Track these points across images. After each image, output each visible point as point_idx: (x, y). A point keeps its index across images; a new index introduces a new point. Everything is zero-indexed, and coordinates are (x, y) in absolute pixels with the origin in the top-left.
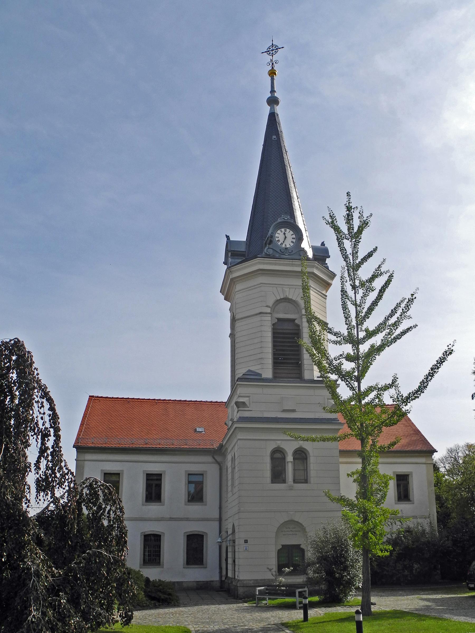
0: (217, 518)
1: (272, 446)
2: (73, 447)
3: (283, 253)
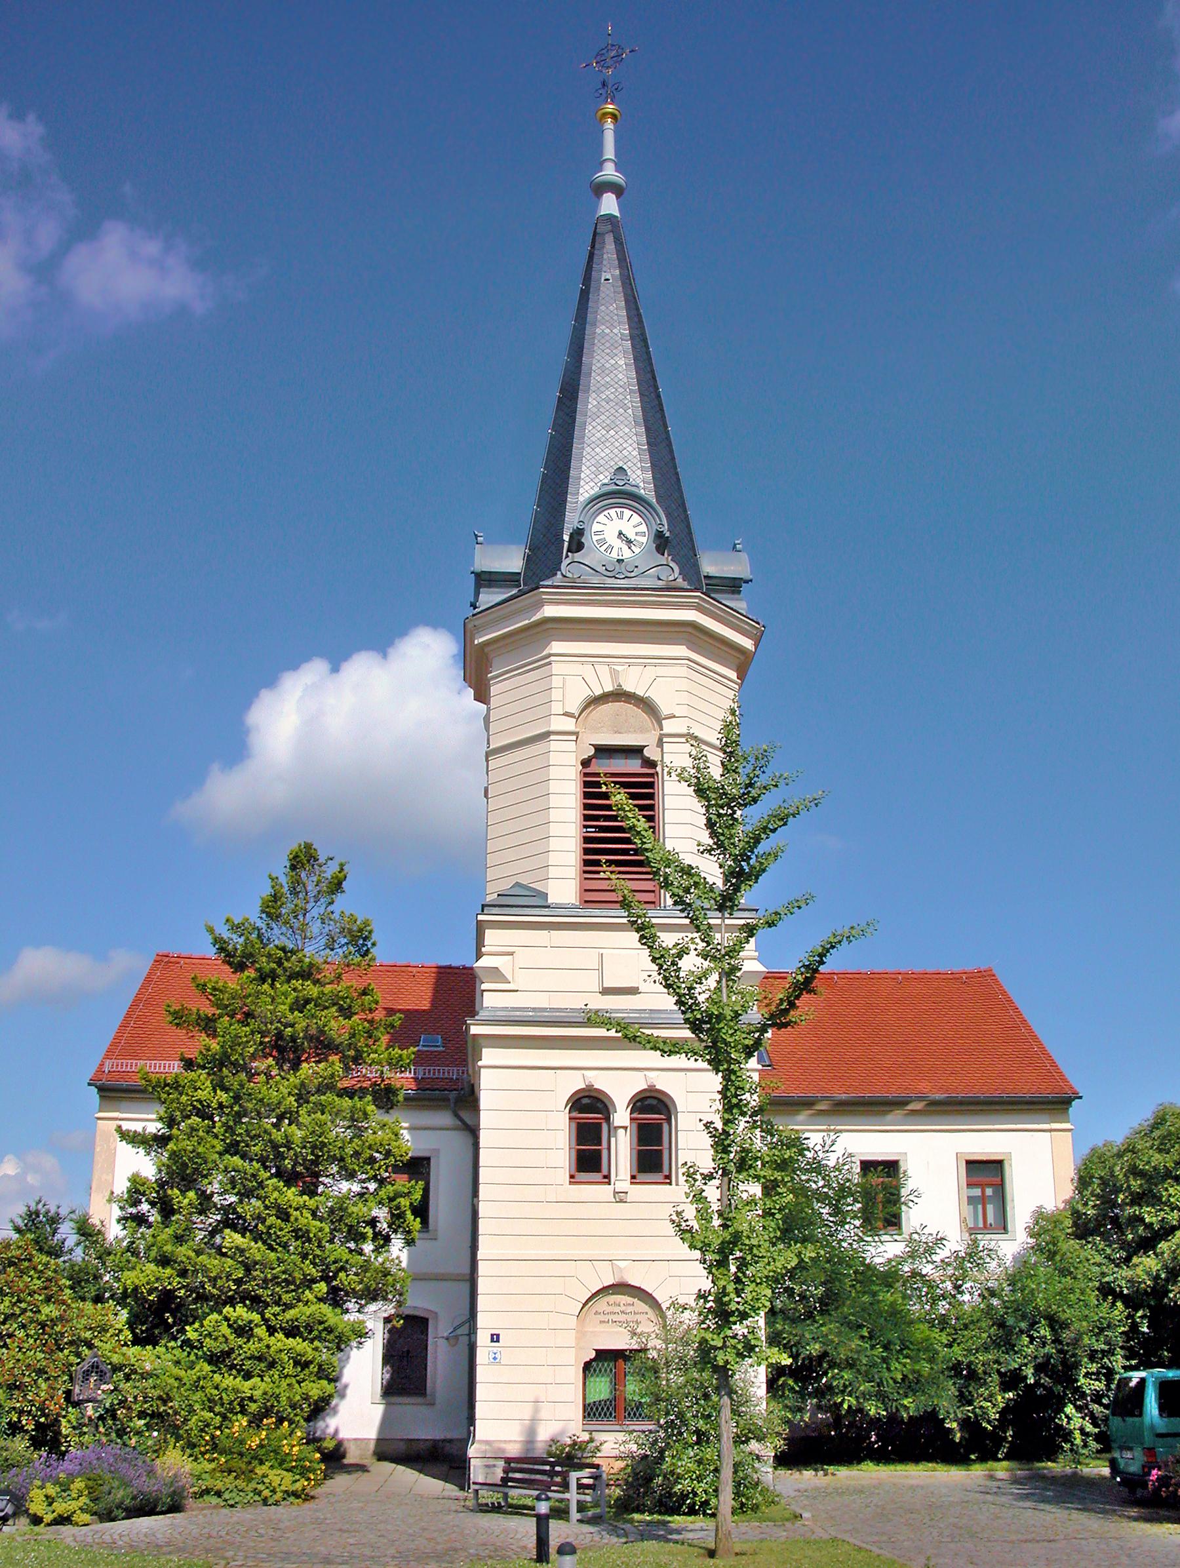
0: (464, 1275)
1: (574, 1083)
2: (90, 1084)
3: (609, 574)
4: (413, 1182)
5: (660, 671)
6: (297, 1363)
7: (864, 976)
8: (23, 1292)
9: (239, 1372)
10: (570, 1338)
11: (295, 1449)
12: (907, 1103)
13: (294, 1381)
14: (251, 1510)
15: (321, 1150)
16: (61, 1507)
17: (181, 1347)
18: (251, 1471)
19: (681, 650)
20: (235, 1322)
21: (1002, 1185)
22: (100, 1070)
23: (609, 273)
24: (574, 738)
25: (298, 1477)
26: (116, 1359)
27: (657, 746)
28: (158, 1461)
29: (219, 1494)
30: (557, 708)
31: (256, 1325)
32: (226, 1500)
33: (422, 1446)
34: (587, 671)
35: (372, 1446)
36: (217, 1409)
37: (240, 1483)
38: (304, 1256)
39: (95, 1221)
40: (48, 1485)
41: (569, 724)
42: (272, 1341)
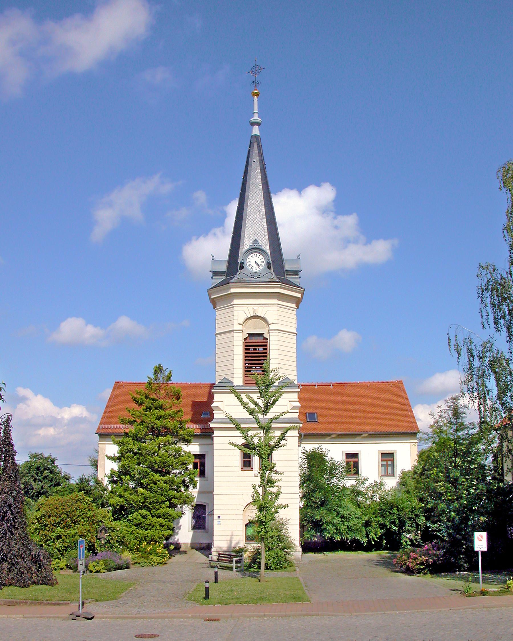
3: (252, 277)
4: (195, 470)
5: (269, 308)
6: (160, 526)
7: (357, 384)
8: (82, 508)
9: (144, 528)
10: (241, 517)
11: (160, 551)
12: (361, 435)
13: (160, 531)
14: (148, 568)
15: (166, 464)
16: (97, 568)
17: (127, 521)
18: (148, 557)
19: (275, 301)
20: (142, 514)
21: (393, 461)
22: (99, 428)
23: (255, 159)
24: (241, 331)
25: (161, 558)
26: (109, 526)
27: (268, 333)
28: (122, 555)
29: (139, 563)
30: (236, 322)
31: (148, 515)
32: (141, 565)
33: (205, 545)
34: (245, 309)
35: (189, 545)
36: (138, 539)
37: (145, 560)
38: (162, 495)
39: (100, 479)
40: (94, 562)
41: (240, 327)
42: (153, 520)
